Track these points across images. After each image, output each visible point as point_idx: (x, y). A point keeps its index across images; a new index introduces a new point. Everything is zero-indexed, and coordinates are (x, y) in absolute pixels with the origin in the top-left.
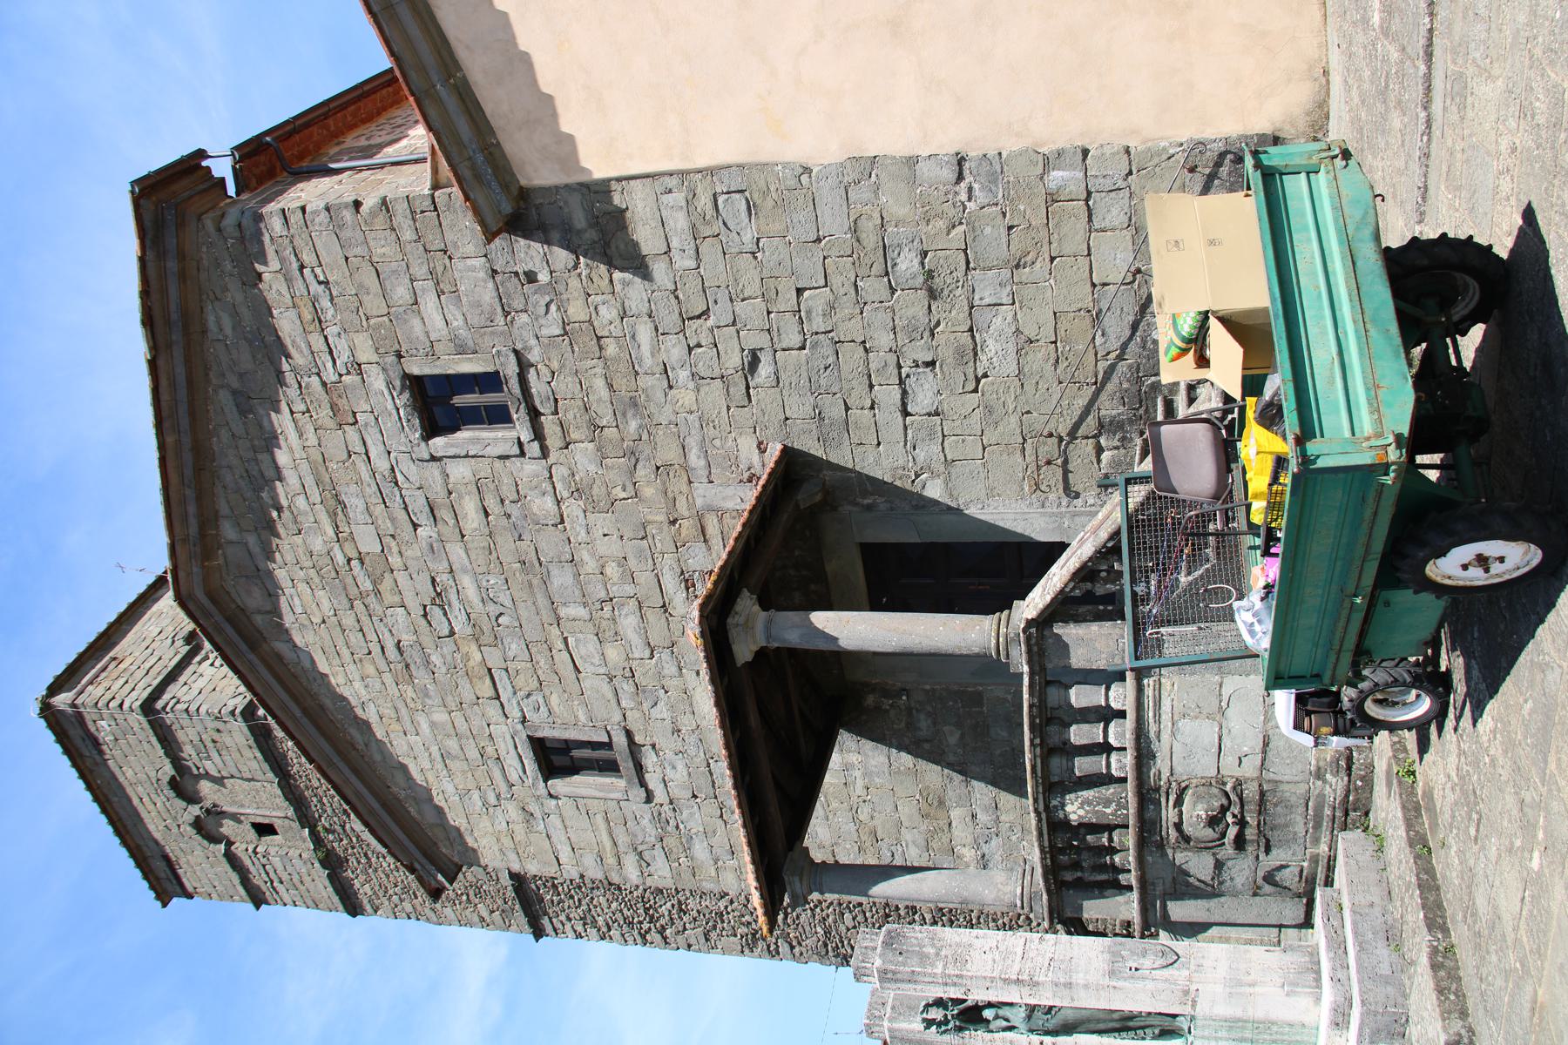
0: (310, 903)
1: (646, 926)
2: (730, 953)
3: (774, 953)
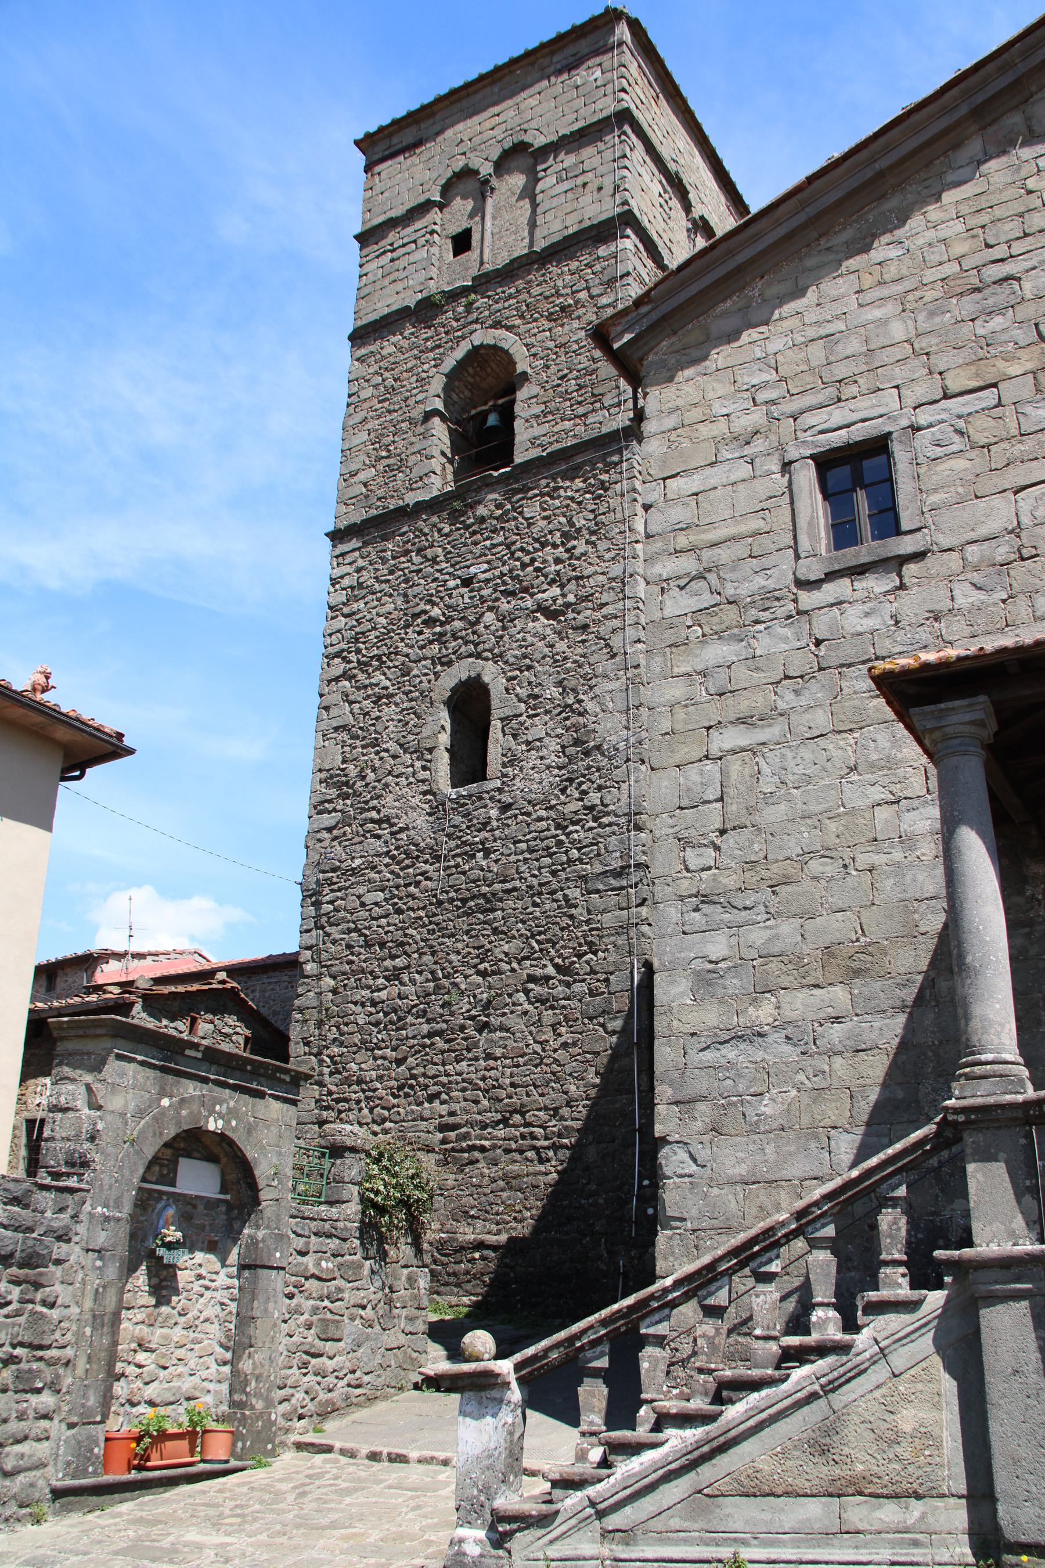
0: (363, 293)
1: (353, 657)
2: (318, 756)
3: (319, 808)
